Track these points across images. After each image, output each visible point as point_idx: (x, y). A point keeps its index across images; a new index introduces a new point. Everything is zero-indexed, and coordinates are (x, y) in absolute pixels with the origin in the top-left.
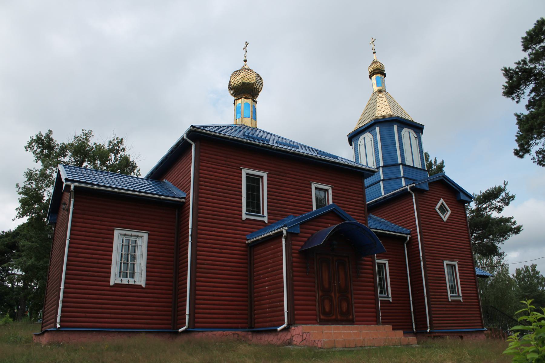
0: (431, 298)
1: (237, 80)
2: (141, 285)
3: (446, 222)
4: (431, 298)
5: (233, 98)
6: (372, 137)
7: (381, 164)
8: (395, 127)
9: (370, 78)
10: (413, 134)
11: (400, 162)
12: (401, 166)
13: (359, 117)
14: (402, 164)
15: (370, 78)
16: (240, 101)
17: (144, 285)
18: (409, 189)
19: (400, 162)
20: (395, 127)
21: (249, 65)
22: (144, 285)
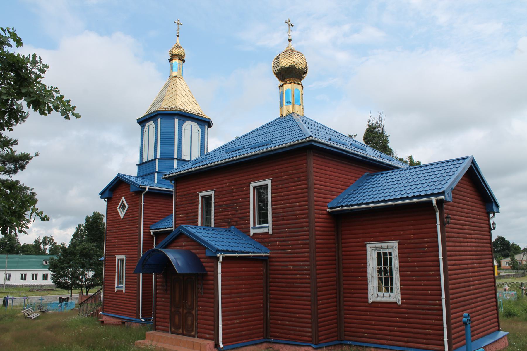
0: (135, 296)
1: (286, 63)
2: (396, 303)
3: (273, 233)
4: (135, 296)
5: (280, 83)
6: (200, 130)
7: (158, 156)
8: (177, 120)
9: (43, 77)
10: (196, 127)
11: (176, 156)
12: (176, 161)
13: (149, 108)
14: (177, 159)
15: (43, 77)
16: (286, 87)
17: (399, 303)
18: (434, 203)
19: (176, 156)
20: (177, 120)
21: (293, 46)
22: (399, 303)
